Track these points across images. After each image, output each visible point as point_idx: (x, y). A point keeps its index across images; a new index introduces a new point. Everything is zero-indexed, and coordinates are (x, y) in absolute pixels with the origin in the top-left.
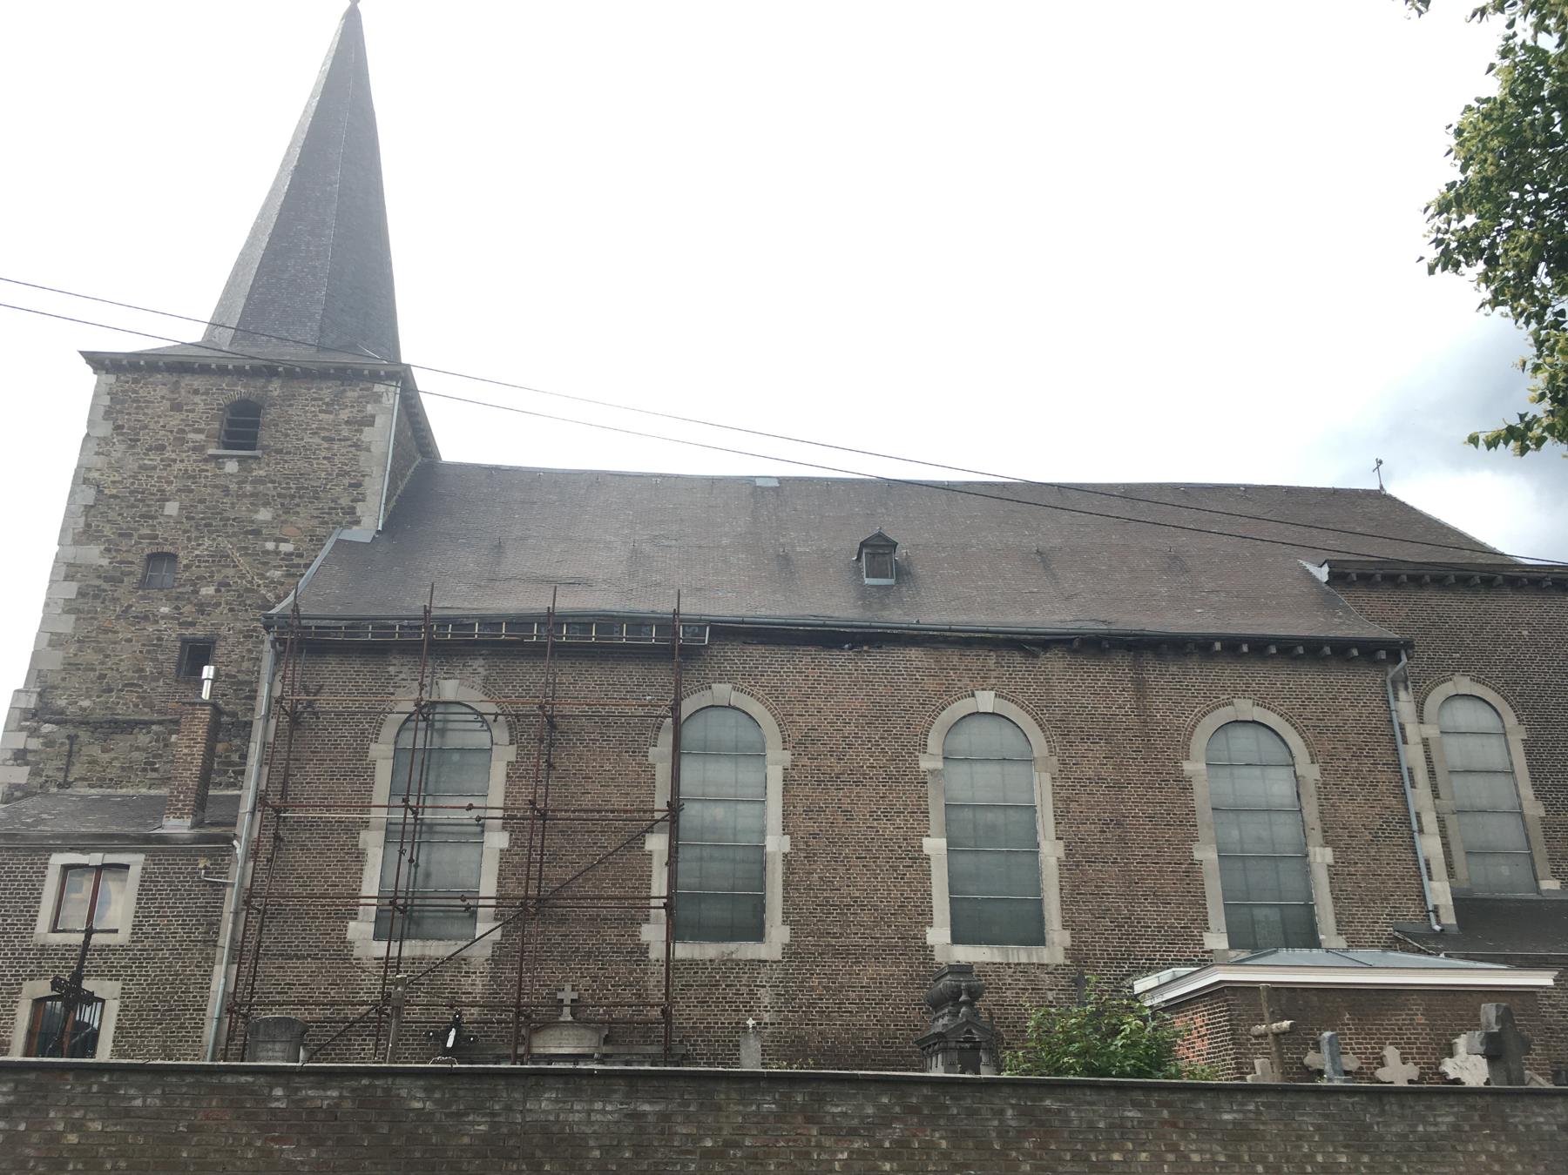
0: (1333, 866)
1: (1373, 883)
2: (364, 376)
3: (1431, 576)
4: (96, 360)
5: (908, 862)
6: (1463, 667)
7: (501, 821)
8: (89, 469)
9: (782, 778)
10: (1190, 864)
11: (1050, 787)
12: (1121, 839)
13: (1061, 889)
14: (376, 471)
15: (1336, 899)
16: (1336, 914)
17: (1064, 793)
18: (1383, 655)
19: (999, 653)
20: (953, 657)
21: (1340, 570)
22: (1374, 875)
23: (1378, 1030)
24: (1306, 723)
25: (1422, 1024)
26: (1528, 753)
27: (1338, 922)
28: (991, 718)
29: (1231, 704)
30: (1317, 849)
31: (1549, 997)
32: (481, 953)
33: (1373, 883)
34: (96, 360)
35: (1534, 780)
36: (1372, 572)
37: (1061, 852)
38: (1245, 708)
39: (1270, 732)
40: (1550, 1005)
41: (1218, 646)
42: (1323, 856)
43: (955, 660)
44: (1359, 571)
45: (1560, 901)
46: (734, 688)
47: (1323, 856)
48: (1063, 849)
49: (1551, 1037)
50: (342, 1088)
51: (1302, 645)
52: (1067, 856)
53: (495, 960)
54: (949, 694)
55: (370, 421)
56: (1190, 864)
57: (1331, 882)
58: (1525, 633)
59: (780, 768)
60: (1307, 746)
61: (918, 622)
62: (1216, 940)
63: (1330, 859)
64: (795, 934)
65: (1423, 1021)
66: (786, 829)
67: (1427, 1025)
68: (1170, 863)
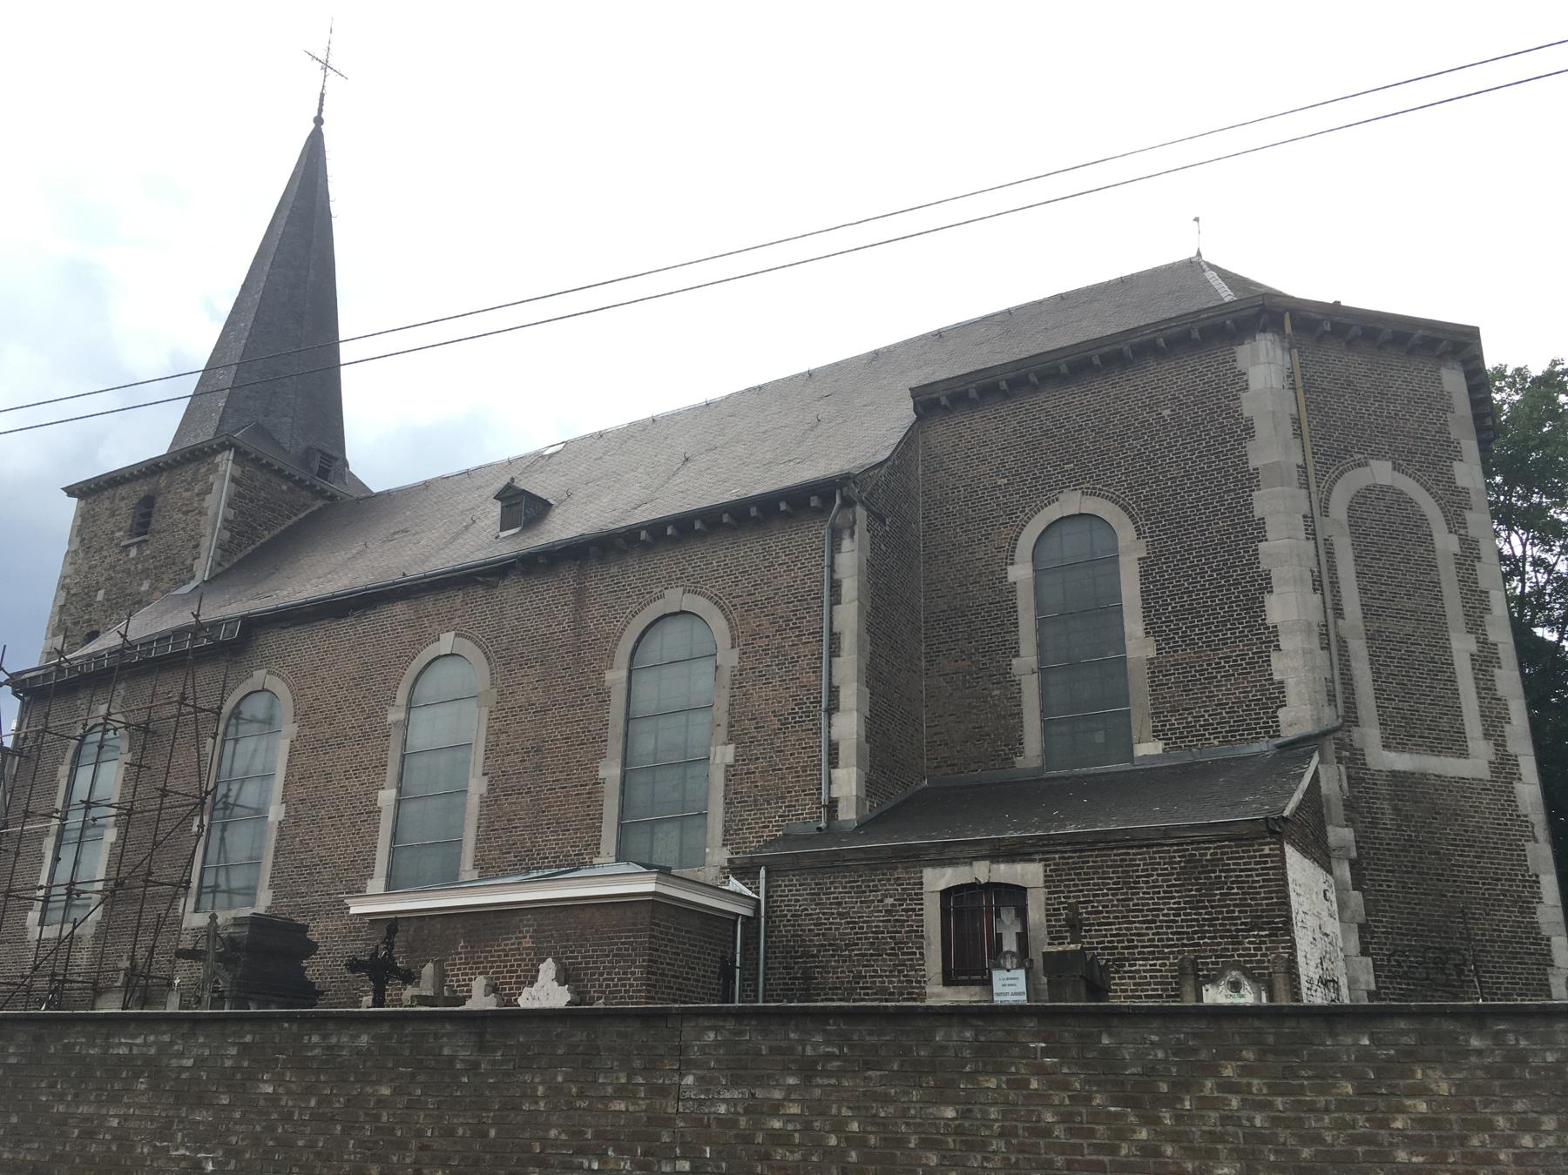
0: (732, 766)
1: (771, 781)
2: (206, 453)
3: (1007, 381)
4: (71, 491)
5: (364, 817)
6: (1074, 482)
7: (114, 818)
8: (65, 578)
9: (288, 751)
10: (594, 784)
11: (486, 720)
12: (538, 767)
13: (479, 827)
14: (209, 531)
15: (729, 804)
16: (726, 821)
17: (497, 726)
18: (814, 501)
19: (465, 591)
20: (428, 604)
21: (927, 397)
22: (773, 770)
23: (486, 957)
24: (735, 601)
25: (528, 948)
26: (1145, 575)
27: (726, 831)
28: (451, 657)
29: (662, 596)
30: (719, 748)
31: (839, 904)
32: (87, 930)
33: (771, 781)
34: (71, 491)
35: (1147, 609)
36: (963, 389)
37: (484, 789)
38: (675, 599)
39: (660, 623)
40: (839, 914)
41: (698, 525)
42: (723, 755)
43: (430, 606)
44: (949, 392)
45: (1169, 767)
46: (268, 673)
47: (723, 755)
48: (485, 785)
49: (833, 956)
50: (1520, 1078)
51: (725, 512)
52: (489, 791)
53: (96, 937)
54: (422, 641)
55: (208, 490)
56: (594, 784)
57: (727, 785)
58: (1166, 413)
59: (288, 741)
60: (731, 628)
61: (404, 575)
62: (468, 871)
63: (730, 759)
64: (275, 897)
65: (531, 945)
66: (285, 800)
67: (533, 949)
68: (576, 786)
